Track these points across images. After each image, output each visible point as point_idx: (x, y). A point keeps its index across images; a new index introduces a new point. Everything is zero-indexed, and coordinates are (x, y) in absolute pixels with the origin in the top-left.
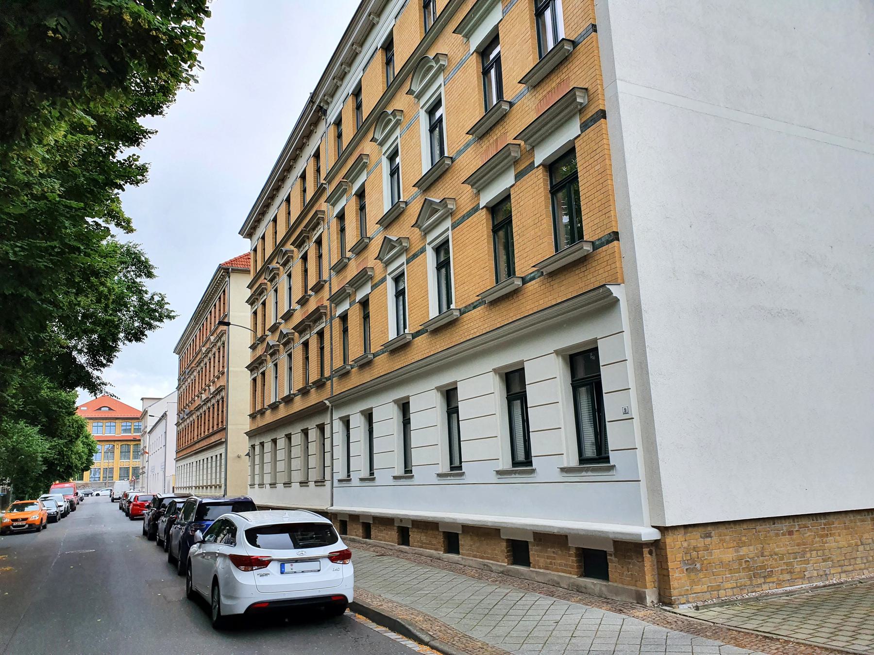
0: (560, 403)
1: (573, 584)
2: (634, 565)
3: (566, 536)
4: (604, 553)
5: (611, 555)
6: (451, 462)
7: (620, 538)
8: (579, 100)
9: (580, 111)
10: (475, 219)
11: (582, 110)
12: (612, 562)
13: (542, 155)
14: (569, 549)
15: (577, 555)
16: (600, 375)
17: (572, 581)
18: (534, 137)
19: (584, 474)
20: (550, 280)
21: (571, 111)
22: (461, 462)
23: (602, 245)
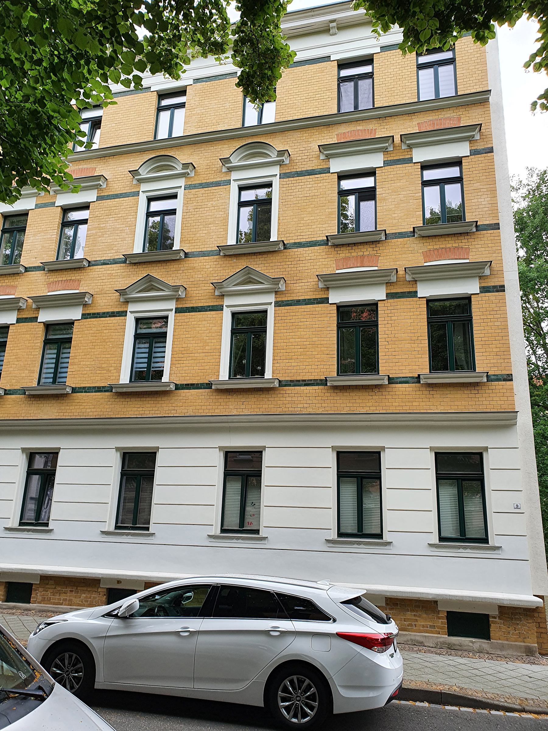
0: (17, 483)
1: (444, 643)
2: (523, 625)
3: (436, 602)
4: (487, 616)
5: (495, 618)
6: (21, 518)
7: (506, 603)
8: (86, 299)
9: (84, 305)
10: (317, 309)
11: (85, 305)
12: (495, 623)
13: (45, 316)
14: (439, 612)
15: (448, 618)
16: (56, 470)
17: (441, 640)
18: (5, 306)
19: (461, 550)
20: (424, 389)
21: (79, 302)
22: (48, 520)
23: (286, 386)
